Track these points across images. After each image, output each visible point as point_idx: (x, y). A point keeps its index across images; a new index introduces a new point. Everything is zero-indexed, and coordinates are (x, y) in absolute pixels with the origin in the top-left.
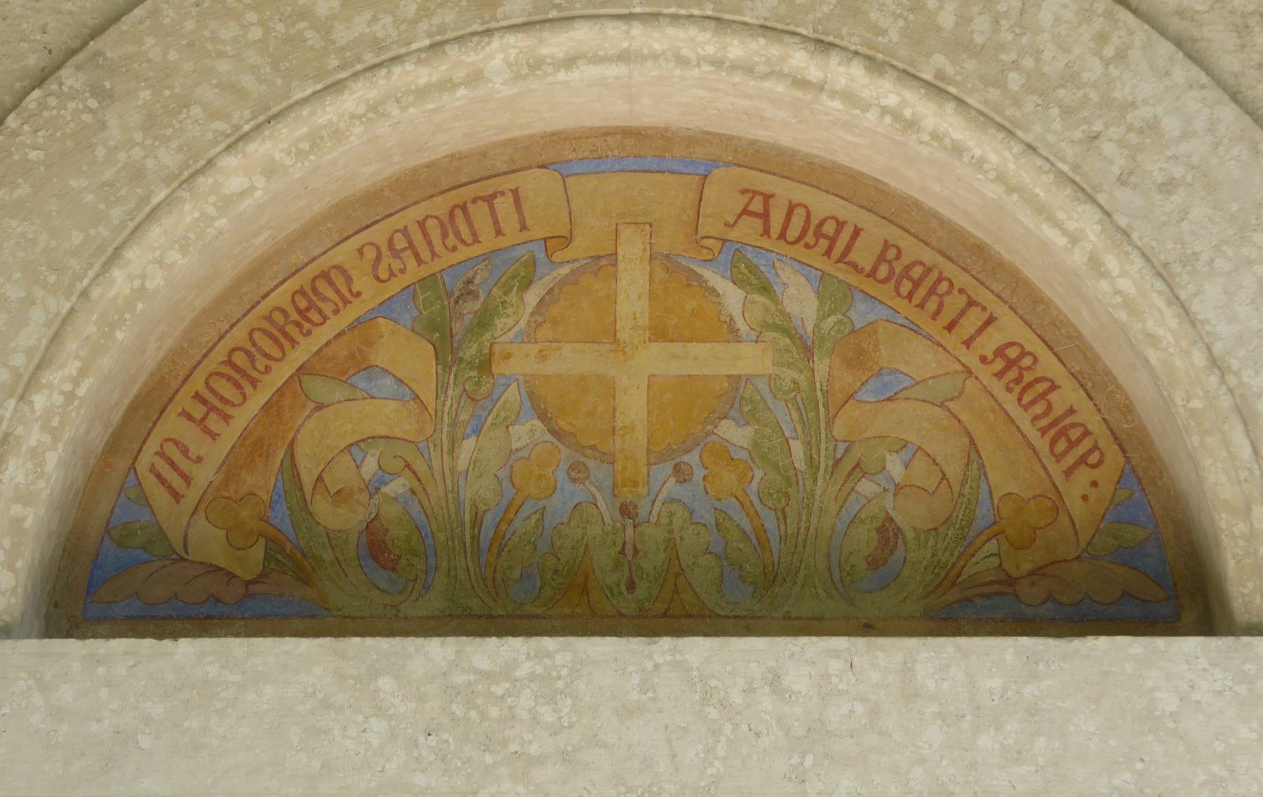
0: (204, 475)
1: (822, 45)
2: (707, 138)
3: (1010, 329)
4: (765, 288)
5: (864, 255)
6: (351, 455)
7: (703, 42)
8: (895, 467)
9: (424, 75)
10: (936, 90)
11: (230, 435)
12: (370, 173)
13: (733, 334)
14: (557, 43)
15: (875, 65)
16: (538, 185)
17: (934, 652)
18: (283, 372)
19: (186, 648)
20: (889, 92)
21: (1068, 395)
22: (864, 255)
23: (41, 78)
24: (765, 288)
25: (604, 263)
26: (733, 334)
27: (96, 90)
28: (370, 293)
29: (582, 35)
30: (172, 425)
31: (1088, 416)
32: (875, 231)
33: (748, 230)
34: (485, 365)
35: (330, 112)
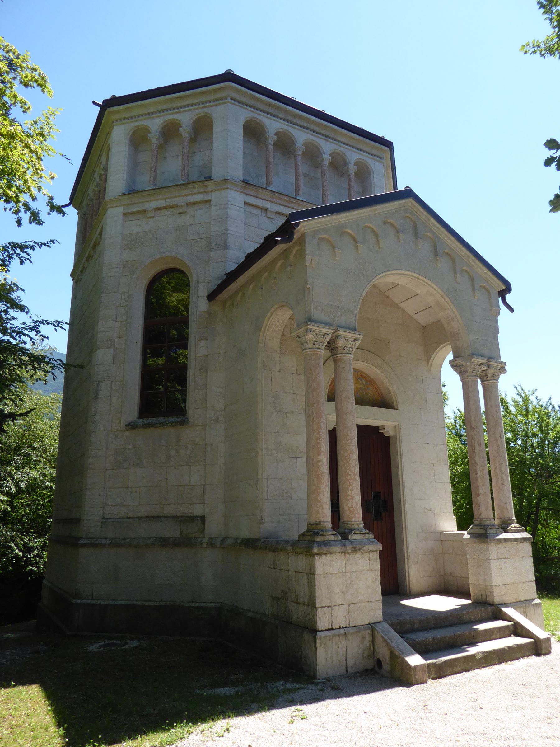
1: (372, 365)
7: (365, 363)
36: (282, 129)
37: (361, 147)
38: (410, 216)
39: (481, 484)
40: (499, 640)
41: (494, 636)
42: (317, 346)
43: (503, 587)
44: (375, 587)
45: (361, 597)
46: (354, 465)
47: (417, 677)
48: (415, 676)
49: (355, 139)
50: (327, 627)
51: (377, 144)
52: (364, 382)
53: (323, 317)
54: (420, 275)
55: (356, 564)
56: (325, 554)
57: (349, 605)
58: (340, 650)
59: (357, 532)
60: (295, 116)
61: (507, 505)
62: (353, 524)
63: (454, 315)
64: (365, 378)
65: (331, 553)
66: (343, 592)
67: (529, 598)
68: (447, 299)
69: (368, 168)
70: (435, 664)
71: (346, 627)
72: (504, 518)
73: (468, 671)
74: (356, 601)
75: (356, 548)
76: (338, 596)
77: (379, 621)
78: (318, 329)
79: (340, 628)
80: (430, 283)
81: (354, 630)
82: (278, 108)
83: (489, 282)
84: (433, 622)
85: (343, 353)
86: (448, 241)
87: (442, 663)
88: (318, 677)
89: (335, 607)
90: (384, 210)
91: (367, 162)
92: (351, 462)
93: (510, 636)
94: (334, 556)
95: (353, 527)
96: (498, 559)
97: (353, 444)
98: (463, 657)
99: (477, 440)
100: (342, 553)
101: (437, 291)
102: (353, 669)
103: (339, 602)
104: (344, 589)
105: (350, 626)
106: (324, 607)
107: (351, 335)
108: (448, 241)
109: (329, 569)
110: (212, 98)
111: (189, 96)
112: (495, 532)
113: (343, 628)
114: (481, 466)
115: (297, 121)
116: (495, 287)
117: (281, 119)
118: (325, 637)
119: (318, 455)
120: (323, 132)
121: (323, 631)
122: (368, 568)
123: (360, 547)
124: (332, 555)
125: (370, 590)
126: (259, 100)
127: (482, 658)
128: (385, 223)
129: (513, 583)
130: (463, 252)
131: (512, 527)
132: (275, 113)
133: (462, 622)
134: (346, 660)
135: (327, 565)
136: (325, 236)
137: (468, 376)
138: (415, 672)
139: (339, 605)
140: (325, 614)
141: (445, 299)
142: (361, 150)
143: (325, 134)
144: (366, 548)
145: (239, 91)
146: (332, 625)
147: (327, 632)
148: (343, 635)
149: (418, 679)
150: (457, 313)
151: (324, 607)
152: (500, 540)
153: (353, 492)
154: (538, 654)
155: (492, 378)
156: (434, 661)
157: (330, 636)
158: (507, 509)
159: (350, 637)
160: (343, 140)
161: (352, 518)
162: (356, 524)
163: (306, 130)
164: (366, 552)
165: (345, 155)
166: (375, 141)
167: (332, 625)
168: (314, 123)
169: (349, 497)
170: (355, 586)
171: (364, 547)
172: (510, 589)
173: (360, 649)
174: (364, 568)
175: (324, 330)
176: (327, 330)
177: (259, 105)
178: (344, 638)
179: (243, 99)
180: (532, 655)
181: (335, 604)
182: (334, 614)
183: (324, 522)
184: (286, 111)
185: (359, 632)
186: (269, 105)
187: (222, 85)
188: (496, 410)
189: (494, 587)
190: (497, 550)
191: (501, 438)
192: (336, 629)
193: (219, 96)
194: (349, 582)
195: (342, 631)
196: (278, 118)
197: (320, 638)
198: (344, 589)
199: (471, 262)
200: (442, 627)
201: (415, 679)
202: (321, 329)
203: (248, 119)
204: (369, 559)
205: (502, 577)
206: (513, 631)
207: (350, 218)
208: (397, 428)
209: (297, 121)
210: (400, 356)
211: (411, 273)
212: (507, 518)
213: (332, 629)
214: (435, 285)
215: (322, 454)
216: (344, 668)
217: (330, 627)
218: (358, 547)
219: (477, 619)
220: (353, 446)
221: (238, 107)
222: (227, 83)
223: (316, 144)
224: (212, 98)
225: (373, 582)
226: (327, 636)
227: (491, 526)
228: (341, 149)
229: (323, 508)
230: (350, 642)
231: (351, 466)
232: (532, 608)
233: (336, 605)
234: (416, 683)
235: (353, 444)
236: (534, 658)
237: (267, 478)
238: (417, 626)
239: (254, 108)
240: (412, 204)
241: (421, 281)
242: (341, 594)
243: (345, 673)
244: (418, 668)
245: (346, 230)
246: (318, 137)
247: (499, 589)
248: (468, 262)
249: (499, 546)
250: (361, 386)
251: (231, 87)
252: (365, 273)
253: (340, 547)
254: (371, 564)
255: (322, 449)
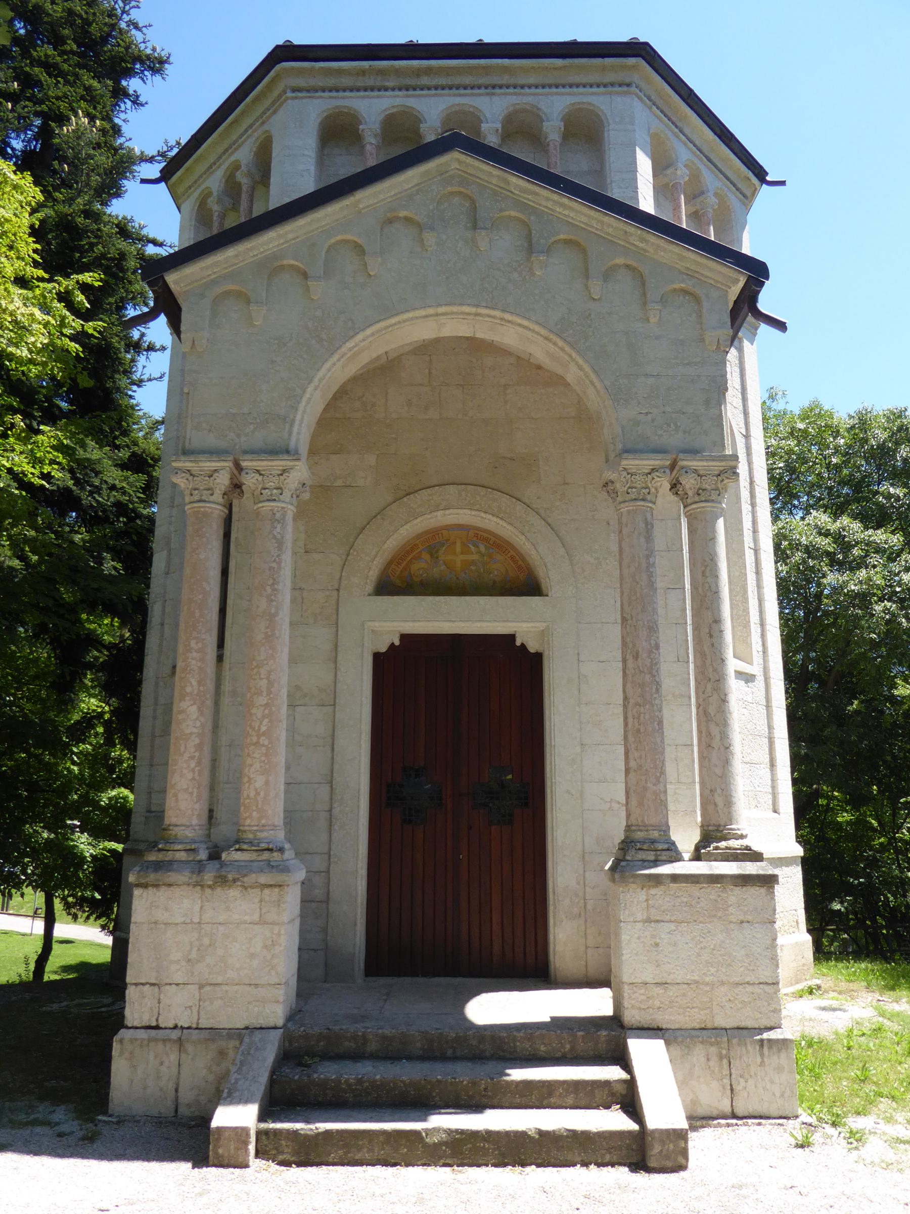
0: (398, 573)
1: (486, 512)
2: (467, 526)
3: (512, 553)
4: (477, 547)
5: (491, 542)
6: (199, 1019)
7: (469, 512)
8: (496, 573)
9: (428, 516)
10: (502, 519)
11: (401, 568)
12: (421, 531)
13: (472, 553)
14: (447, 512)
15: (493, 515)
16: (445, 532)
17: (882, 712)
18: (409, 559)
19: (395, 598)
20: (495, 519)
21: (520, 562)
22: (491, 542)
23: (375, 517)
24: (477, 547)
25: (455, 543)
26: (472, 553)
27: (383, 519)
28: (421, 547)
29: (451, 511)
30: (393, 566)
31: (523, 565)
32: (493, 539)
33: (475, 539)
34: (437, 558)
35: (415, 522)
36: (393, 107)
37: (577, 79)
38: (462, 190)
39: (633, 746)
40: (534, 1111)
41: (553, 1100)
42: (196, 498)
43: (659, 990)
44: (269, 957)
45: (230, 974)
46: (259, 715)
47: (220, 1151)
48: (216, 1147)
49: (555, 69)
50: (145, 1023)
51: (608, 61)
52: (482, 548)
53: (211, 441)
54: (477, 306)
55: (228, 909)
56: (156, 886)
57: (201, 987)
58: (164, 1069)
59: (245, 847)
60: (418, 73)
61: (716, 796)
62: (245, 831)
63: (581, 373)
64: (486, 540)
65: (170, 885)
66: (189, 960)
67: (750, 1024)
68: (560, 343)
69: (598, 116)
70: (295, 1132)
71: (189, 1028)
72: (708, 826)
73: (394, 1165)
74: (220, 980)
75: (225, 877)
76: (178, 967)
77: (272, 1024)
78: (194, 465)
79: (176, 1027)
80: (507, 316)
81: (205, 1034)
82: (381, 72)
83: (697, 275)
84: (418, 1045)
85: (261, 502)
86: (566, 212)
87: (318, 1134)
88: (110, 1112)
89: (168, 987)
90: (382, 197)
91: (594, 105)
92: (254, 711)
93: (607, 1107)
94: (177, 892)
95: (245, 836)
96: (648, 921)
97: (262, 676)
98: (384, 1132)
99: (631, 646)
100: (194, 886)
101: (533, 331)
102: (192, 1110)
103: (179, 977)
104: (194, 955)
105: (200, 1026)
106: (143, 984)
107: (270, 463)
108: (566, 212)
109: (161, 915)
110: (268, 103)
111: (243, 113)
112: (652, 858)
113: (182, 1028)
114: (637, 704)
115: (425, 80)
116: (717, 282)
117: (393, 89)
118: (132, 1041)
119: (180, 701)
120: (483, 81)
121: (137, 1028)
122: (256, 917)
123: (237, 876)
124: (172, 888)
125: (255, 963)
126: (340, 72)
127: (441, 1143)
128: (390, 221)
129: (696, 982)
130: (609, 225)
131: (717, 848)
132: (378, 84)
133: (508, 1056)
134: (177, 1090)
135: (157, 907)
136: (231, 287)
137: (620, 503)
138: (218, 1140)
139: (177, 985)
140: (144, 997)
141: (555, 344)
142: (578, 86)
143: (488, 83)
144: (251, 879)
145: (301, 72)
146: (157, 1020)
147: (143, 1031)
148: (175, 1041)
149: (222, 1156)
150: (587, 368)
151: (143, 984)
152: (657, 880)
153: (252, 769)
154: (639, 1165)
155: (697, 498)
156: (298, 1126)
157: (143, 1040)
158: (716, 805)
159: (190, 1048)
160: (532, 80)
161: (245, 819)
162: (250, 831)
163: (446, 92)
164: (252, 887)
165: (538, 109)
166: (603, 56)
167: (157, 1020)
168: (458, 71)
169: (246, 779)
170: (220, 952)
171: (245, 875)
172: (684, 995)
173: (211, 1073)
174: (247, 918)
175: (208, 464)
176: (214, 464)
177: (346, 81)
178: (176, 1048)
179: (312, 82)
180: (620, 1164)
181: (168, 981)
182: (165, 1000)
183: (176, 826)
184: (398, 72)
185: (213, 1040)
186: (363, 72)
187: (272, 73)
188: (703, 572)
189: (626, 987)
190: (647, 900)
191: (711, 636)
192: (166, 1028)
193: (276, 93)
194: (206, 941)
195: (175, 1035)
196: (386, 89)
197: (121, 1041)
198: (194, 955)
199: (637, 243)
200: (443, 1058)
201: (216, 1153)
202: (201, 464)
203: (325, 114)
204: (261, 901)
205: (658, 966)
206: (623, 1096)
207: (290, 236)
208: (543, 634)
209: (425, 80)
210: (565, 484)
211: (455, 309)
212: (714, 825)
213: (157, 1027)
214: (524, 317)
215: (187, 698)
216: (170, 1104)
217: (154, 1024)
218: (230, 877)
219: (559, 1054)
220: (261, 679)
221: (304, 101)
222: (278, 67)
223: (471, 110)
224: (268, 103)
225: (265, 947)
226: (136, 1039)
227: (644, 843)
228: (526, 99)
229: (177, 800)
230: (190, 1057)
231: (254, 718)
232: (753, 1050)
233: (170, 984)
234: (216, 1162)
235: (262, 676)
236: (623, 1172)
237: (230, 746)
238: (372, 1046)
239: (337, 91)
240: (460, 162)
241: (487, 319)
242: (184, 963)
243: (173, 1114)
244: (227, 1134)
245: (285, 262)
246: (472, 95)
247: (643, 991)
248: (627, 245)
249: (653, 891)
250: (475, 557)
251: (285, 70)
252: (324, 337)
253: (187, 874)
254: (264, 911)
255: (188, 689)
